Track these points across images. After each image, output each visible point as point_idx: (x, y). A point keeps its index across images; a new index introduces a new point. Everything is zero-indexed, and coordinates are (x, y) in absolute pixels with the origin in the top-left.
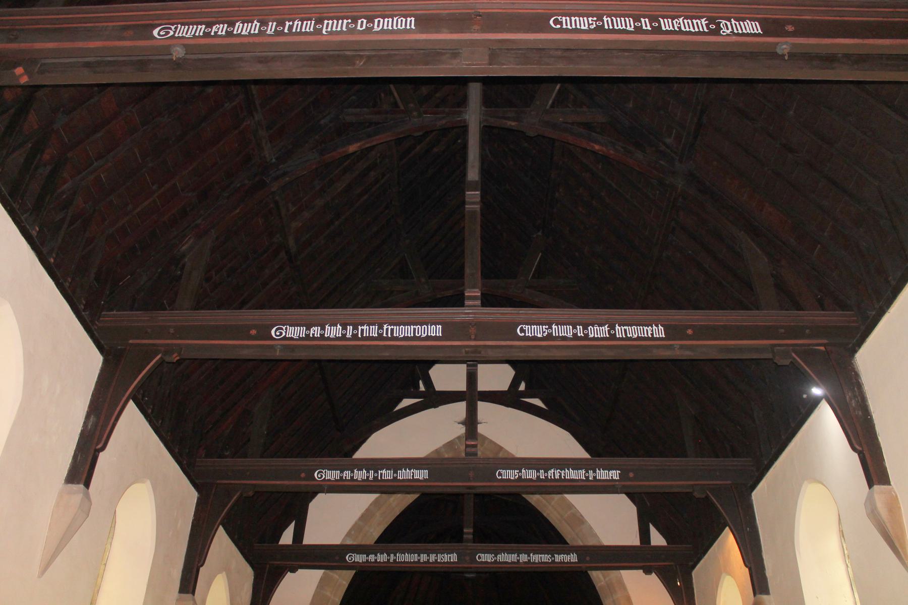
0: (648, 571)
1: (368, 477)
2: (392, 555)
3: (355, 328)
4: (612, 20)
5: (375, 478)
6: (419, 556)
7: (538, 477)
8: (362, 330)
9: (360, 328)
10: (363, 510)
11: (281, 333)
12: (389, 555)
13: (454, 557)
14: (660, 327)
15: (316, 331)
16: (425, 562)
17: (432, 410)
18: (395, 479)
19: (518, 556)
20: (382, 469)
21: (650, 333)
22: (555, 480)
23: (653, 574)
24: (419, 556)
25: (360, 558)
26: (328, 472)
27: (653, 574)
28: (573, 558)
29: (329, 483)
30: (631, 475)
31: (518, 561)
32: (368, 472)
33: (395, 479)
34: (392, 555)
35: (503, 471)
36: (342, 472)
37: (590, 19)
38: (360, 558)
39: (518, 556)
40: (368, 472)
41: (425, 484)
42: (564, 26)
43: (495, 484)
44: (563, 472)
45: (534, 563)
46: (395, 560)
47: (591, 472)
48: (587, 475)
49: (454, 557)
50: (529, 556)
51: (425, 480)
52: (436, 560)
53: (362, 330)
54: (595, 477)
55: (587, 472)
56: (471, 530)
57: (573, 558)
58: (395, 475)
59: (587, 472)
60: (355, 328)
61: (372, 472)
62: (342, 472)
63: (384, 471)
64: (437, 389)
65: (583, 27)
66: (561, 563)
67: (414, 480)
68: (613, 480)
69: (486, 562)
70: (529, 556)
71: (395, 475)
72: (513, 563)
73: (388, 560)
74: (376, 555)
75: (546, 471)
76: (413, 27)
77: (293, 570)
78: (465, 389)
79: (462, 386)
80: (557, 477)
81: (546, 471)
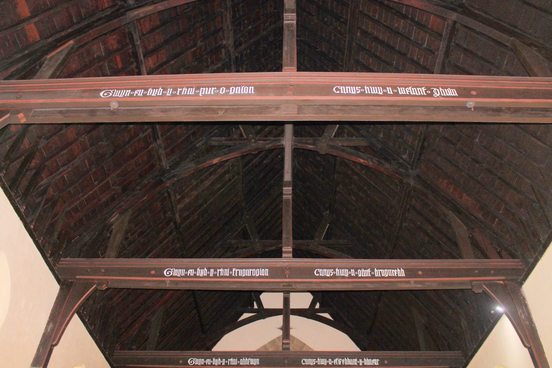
1: (221, 363)
8: (220, 272)
9: (218, 270)
15: (191, 272)
20: (220, 268)
30: (386, 362)
32: (222, 360)
35: (306, 360)
36: (205, 360)
37: (357, 88)
40: (222, 360)
47: (361, 360)
53: (220, 272)
55: (358, 360)
58: (239, 362)
59: (358, 360)
61: (224, 360)
62: (205, 360)
63: (232, 360)
65: (353, 93)
68: (375, 366)
71: (239, 362)
75: (333, 360)
76: (253, 92)
81: (333, 360)
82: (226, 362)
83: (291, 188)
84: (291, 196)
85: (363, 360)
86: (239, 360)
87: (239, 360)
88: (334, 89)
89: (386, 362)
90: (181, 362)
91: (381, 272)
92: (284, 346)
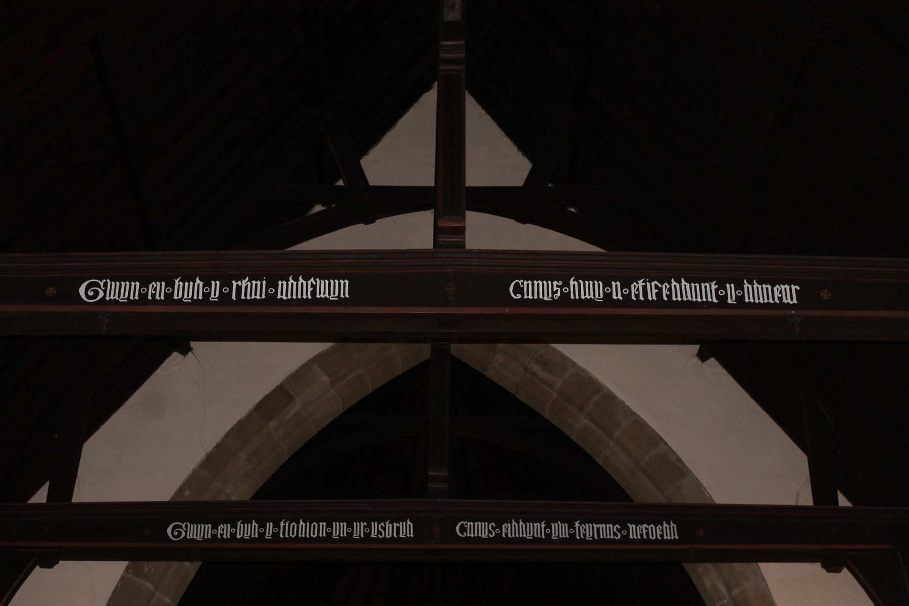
0: (832, 565)
1: (207, 295)
2: (270, 526)
3: (226, 283)
4: (579, 285)
5: (224, 298)
6: (329, 525)
7: (607, 296)
8: (239, 288)
9: (234, 283)
10: (209, 446)
11: (96, 293)
12: (262, 525)
13: (406, 529)
14: (672, 524)
15: (157, 290)
16: (341, 539)
17: (361, 226)
18: (271, 299)
19: (548, 526)
20: (240, 278)
21: (659, 533)
22: (647, 303)
23: (845, 571)
24: (329, 525)
25: (197, 532)
26: (113, 286)
27: (845, 571)
28: (669, 531)
29: (114, 309)
30: (825, 295)
31: (548, 536)
32: (207, 284)
33: (271, 299)
34: (270, 526)
35: (525, 284)
36: (145, 284)
37: (555, 283)
38: (197, 532)
39: (548, 526)
40: (207, 284)
41: (342, 310)
42: (526, 297)
43: (507, 310)
44: (665, 287)
45: (583, 541)
46: (275, 535)
47: (731, 288)
48: (722, 293)
49: (406, 529)
50: (571, 526)
51: (341, 301)
52: (367, 535)
53: (239, 288)
54: (740, 299)
55: (721, 286)
56: (445, 473)
57: (669, 531)
58: (272, 291)
59: (721, 286)
60: (226, 283)
61: (216, 285)
62: (145, 284)
63: (244, 283)
64: (372, 182)
65: (546, 298)
66: (642, 541)
67: (315, 301)
68: (782, 305)
69: (478, 539)
70: (571, 526)
71: (272, 291)
72: (535, 540)
73: (262, 535)
74: (234, 526)
75: (626, 284)
76: (347, 295)
77: (49, 563)
78: (431, 183)
79: (425, 177)
80: (652, 296)
81: (626, 284)
82: (226, 290)
83: (463, 43)
84: (463, 67)
85: (739, 287)
86: (272, 284)
87: (272, 284)
88: (457, 528)
89: (825, 295)
90: (51, 291)
91: (598, 529)
92: (444, 239)
